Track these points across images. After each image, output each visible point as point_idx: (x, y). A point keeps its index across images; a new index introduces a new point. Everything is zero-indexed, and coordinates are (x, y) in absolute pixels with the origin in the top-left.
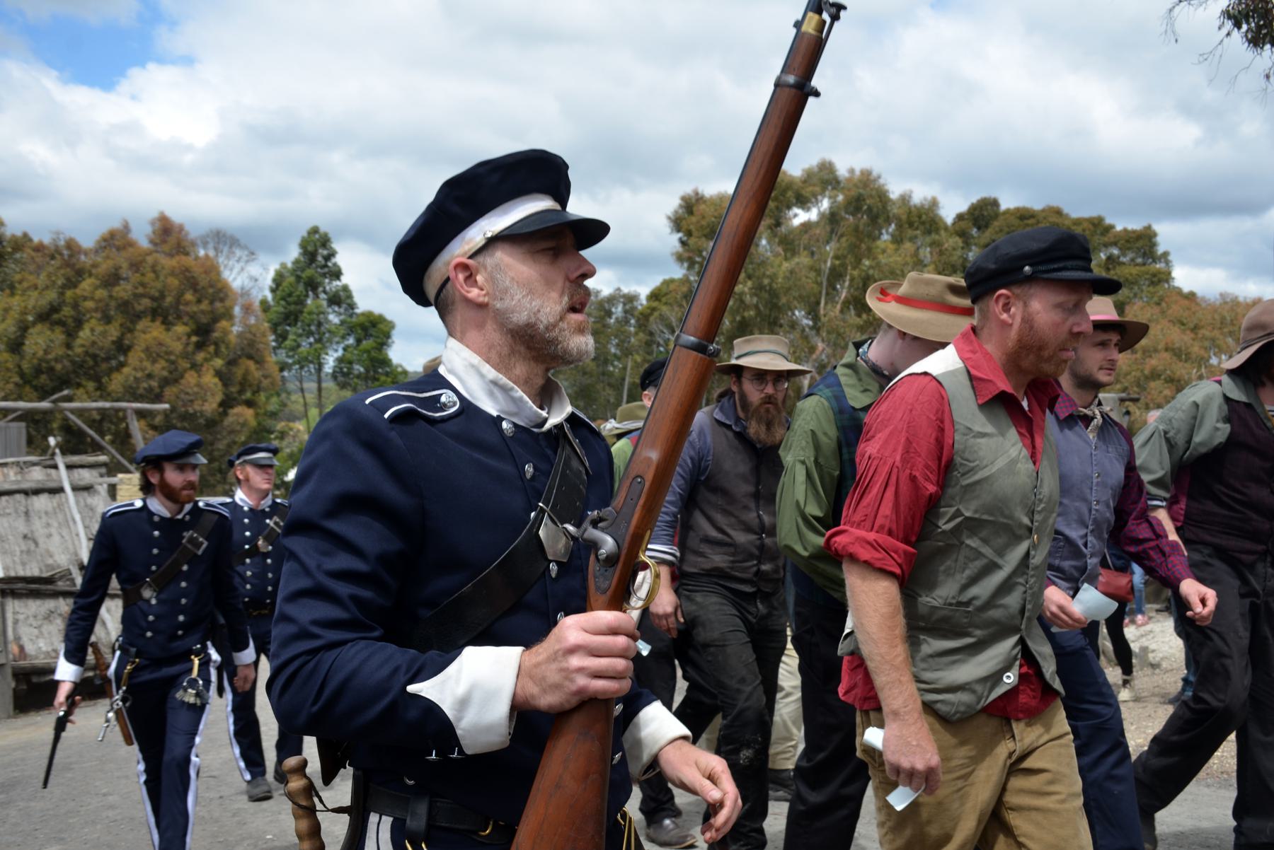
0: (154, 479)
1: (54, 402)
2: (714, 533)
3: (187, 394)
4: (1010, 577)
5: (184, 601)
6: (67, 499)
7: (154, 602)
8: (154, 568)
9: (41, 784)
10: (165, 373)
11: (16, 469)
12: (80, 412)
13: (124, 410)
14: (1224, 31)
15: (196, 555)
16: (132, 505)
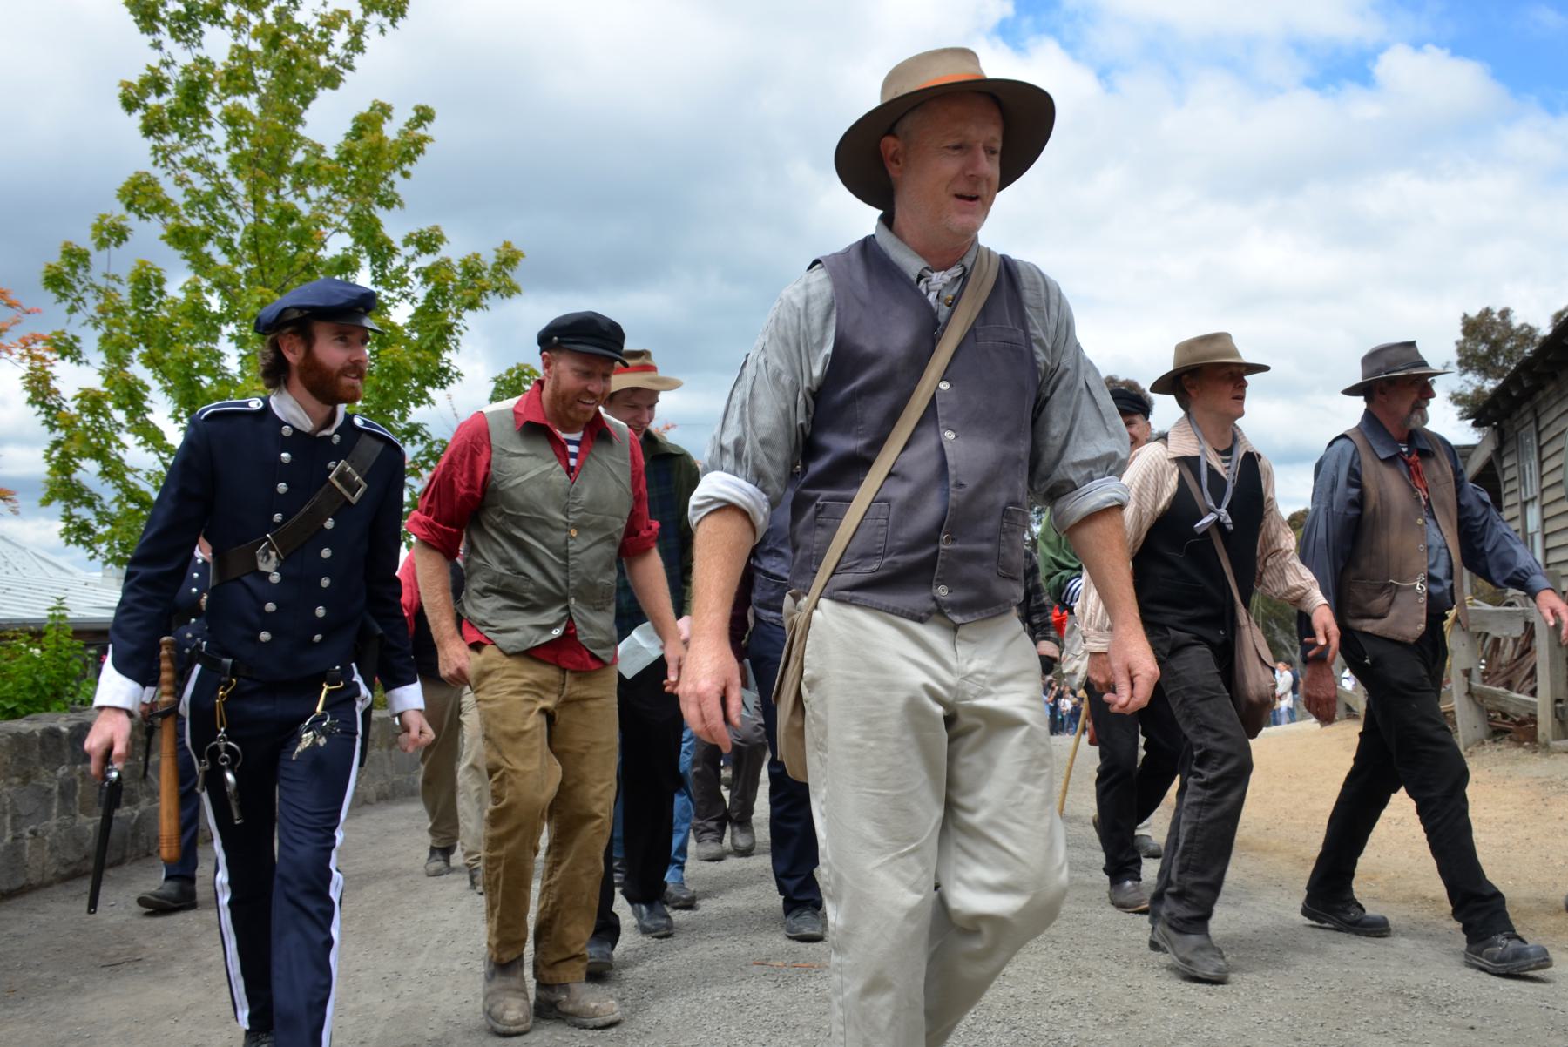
0: (293, 357)
4: (180, 697)
5: (325, 582)
7: (275, 578)
8: (278, 517)
9: (819, 945)
15: (348, 502)
16: (246, 404)
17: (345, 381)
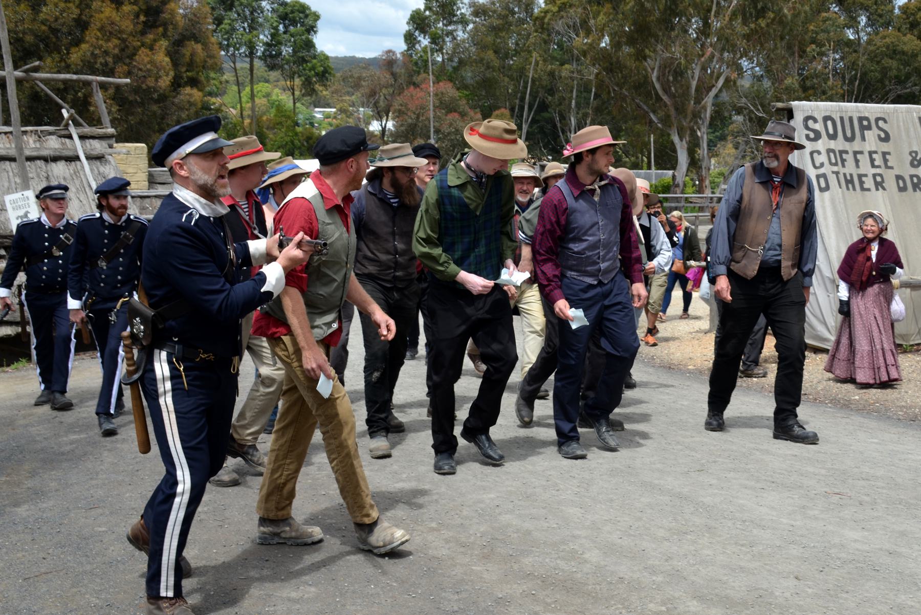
1: (26, 71)
2: (369, 254)
3: (140, 70)
6: (83, 167)
10: (116, 51)
11: (34, 137)
12: (46, 82)
13: (88, 84)
14: (877, 378)
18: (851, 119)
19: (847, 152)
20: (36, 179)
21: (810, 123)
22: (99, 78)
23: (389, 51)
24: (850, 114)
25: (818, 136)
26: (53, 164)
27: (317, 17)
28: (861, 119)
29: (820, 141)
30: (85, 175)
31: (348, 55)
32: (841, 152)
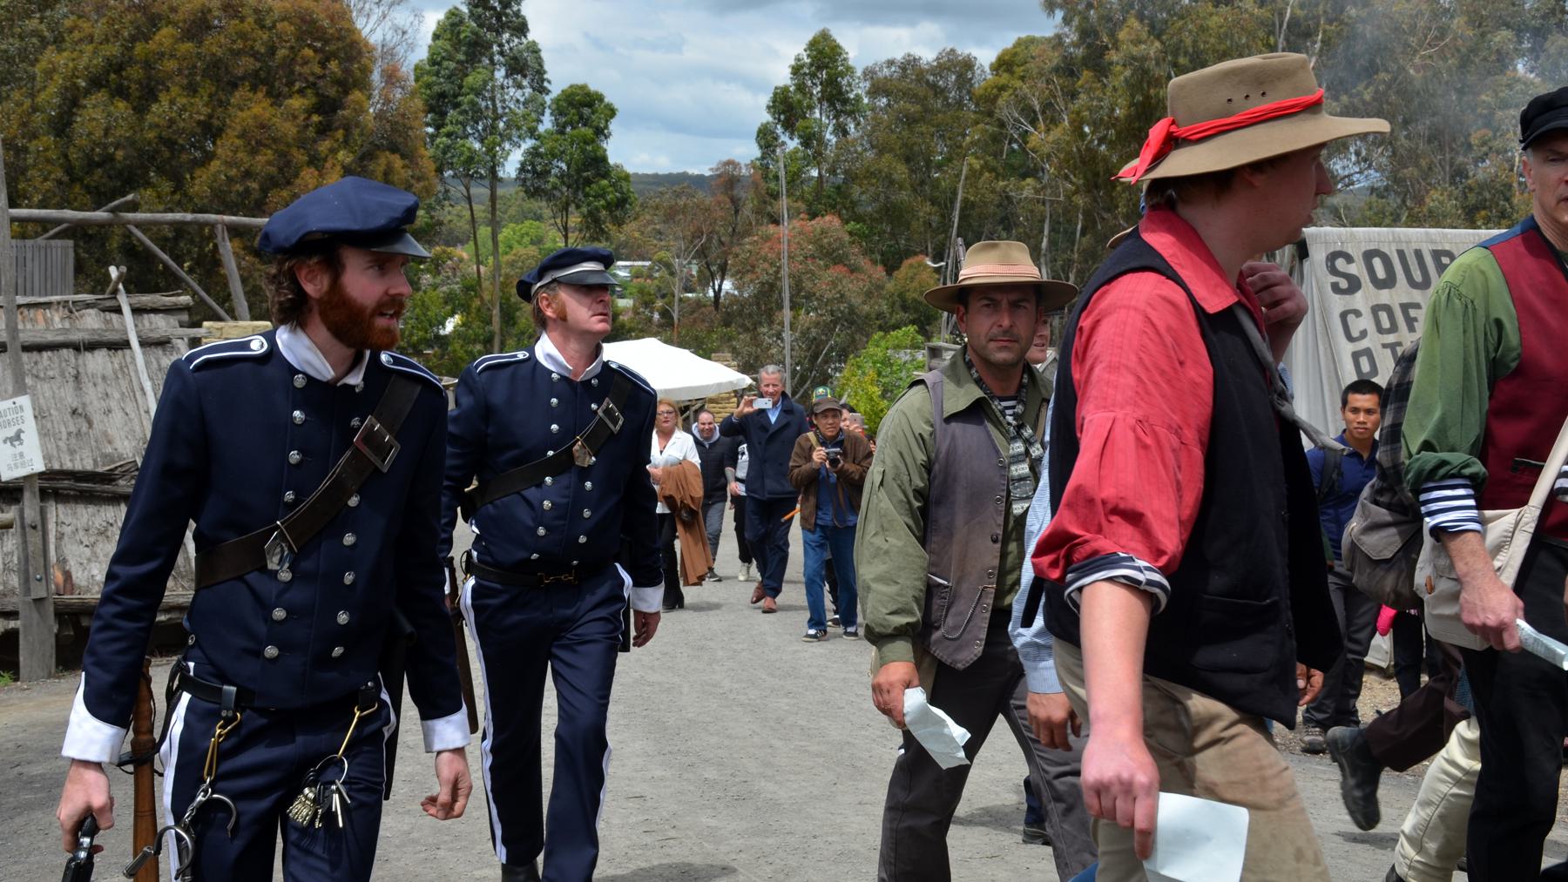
1: (112, 211)
6: (133, 358)
8: (289, 496)
11: (63, 312)
13: (213, 225)
15: (377, 470)
17: (381, 322)
18: (1418, 254)
19: (1417, 306)
20: (59, 379)
21: (1340, 264)
22: (227, 218)
23: (729, 163)
24: (1415, 246)
25: (1354, 285)
26: (88, 355)
27: (612, 112)
28: (1437, 255)
29: (1359, 294)
30: (136, 371)
31: (675, 171)
32: (1405, 307)
